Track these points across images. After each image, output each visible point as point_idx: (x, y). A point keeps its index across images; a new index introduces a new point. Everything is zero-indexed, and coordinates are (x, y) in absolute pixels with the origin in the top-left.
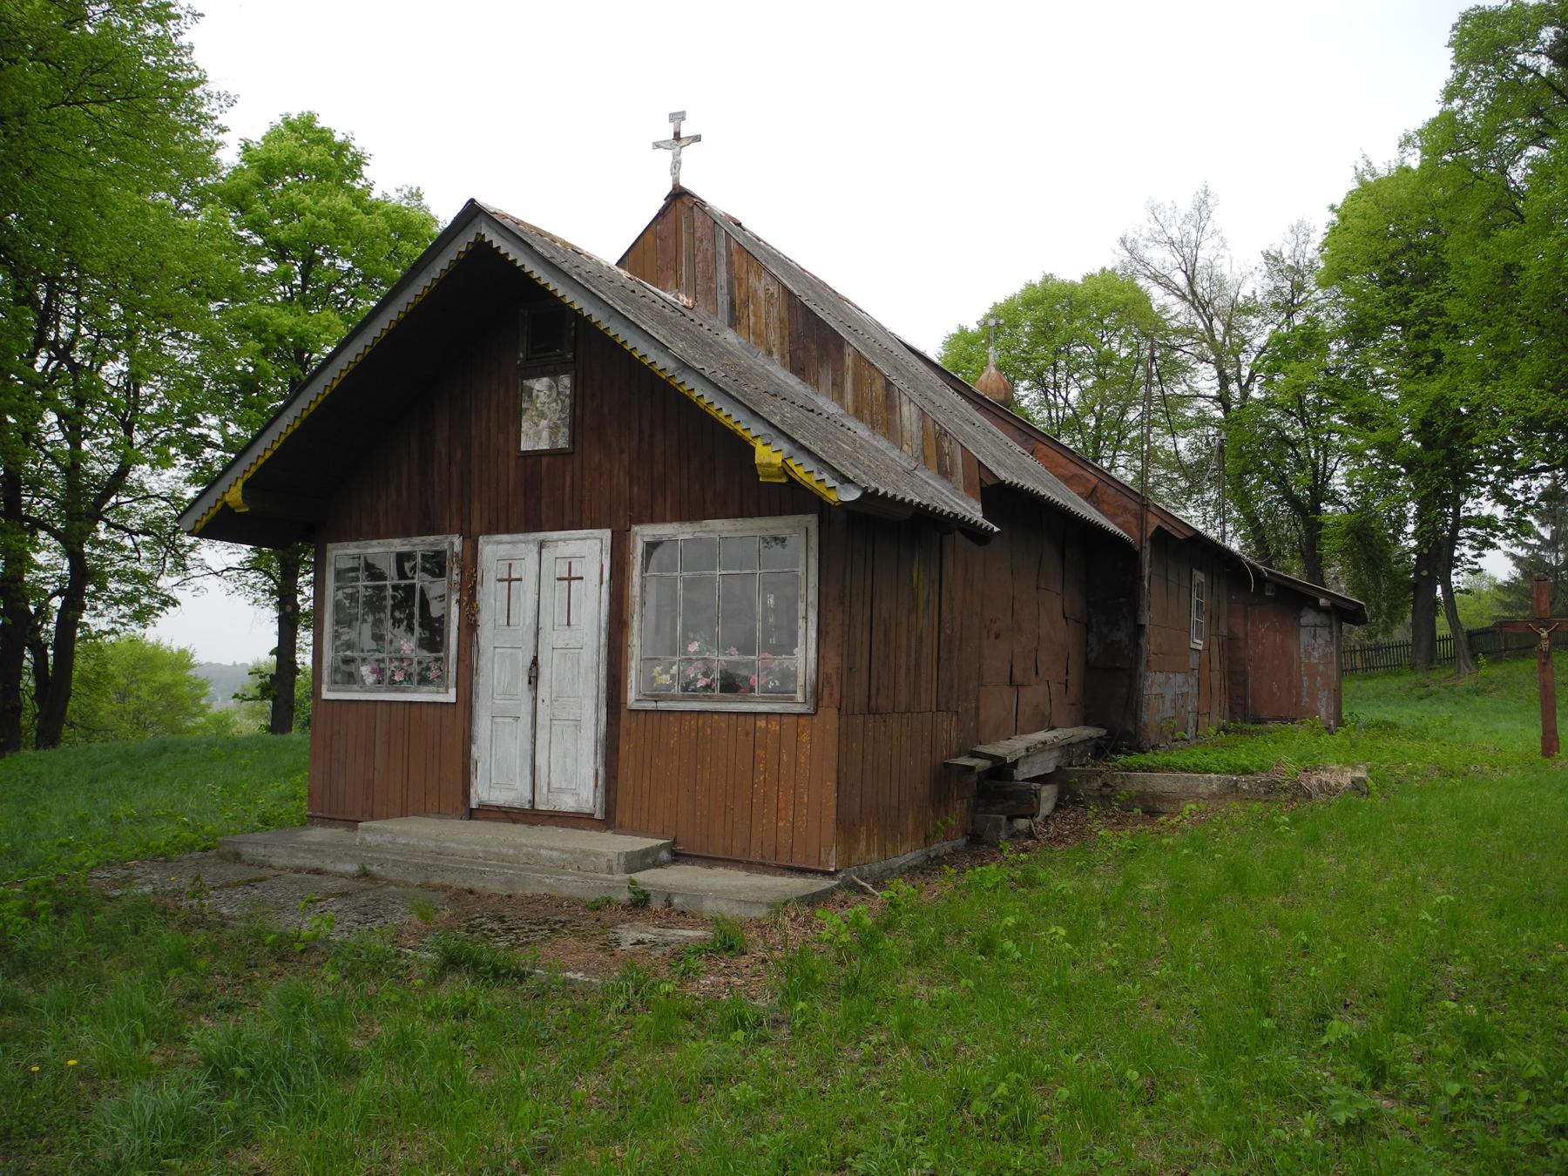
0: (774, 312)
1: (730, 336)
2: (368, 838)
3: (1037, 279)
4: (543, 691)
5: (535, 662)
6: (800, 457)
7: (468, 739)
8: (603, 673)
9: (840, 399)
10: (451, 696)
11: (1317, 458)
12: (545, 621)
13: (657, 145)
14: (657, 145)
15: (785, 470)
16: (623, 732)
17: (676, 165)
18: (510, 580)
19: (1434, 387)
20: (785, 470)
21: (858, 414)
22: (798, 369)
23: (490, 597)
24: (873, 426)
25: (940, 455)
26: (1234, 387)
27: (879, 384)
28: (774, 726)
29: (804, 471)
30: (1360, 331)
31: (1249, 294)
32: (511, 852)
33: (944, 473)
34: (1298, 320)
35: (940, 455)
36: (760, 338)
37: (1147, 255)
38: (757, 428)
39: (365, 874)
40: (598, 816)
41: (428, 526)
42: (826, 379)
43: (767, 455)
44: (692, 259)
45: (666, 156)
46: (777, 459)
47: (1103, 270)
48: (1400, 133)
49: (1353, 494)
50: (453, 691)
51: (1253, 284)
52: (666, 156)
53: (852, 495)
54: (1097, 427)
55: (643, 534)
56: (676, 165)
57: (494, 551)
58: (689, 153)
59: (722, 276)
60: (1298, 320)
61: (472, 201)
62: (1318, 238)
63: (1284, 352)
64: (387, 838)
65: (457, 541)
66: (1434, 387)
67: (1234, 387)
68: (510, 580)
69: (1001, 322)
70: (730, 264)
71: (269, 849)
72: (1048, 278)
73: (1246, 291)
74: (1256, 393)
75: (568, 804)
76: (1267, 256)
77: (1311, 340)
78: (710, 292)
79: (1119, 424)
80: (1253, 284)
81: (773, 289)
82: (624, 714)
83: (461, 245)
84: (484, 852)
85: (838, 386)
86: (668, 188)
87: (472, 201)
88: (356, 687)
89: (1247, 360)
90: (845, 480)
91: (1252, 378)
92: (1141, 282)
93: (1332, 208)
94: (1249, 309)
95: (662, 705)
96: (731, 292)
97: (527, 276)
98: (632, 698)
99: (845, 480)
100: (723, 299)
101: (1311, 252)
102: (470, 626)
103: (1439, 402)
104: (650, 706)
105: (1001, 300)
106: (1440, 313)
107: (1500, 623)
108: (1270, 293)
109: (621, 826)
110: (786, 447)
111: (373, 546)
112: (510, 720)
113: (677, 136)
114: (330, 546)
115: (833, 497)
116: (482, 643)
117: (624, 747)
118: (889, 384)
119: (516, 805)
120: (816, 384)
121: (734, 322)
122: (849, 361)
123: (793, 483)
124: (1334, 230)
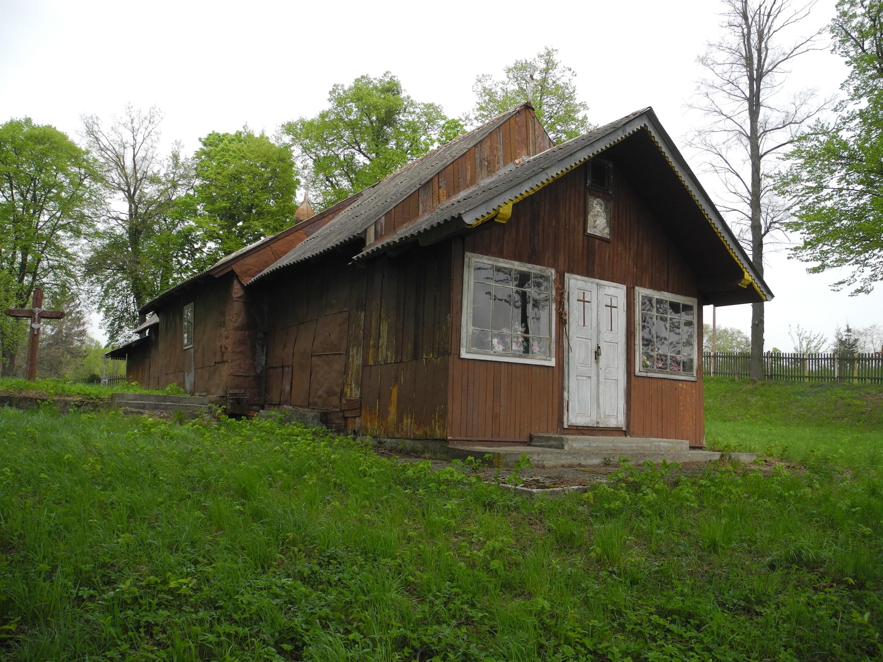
2: (575, 445)
6: (757, 281)
10: (552, 363)
16: (632, 386)
23: (574, 310)
31: (156, 171)
32: (648, 445)
39: (607, 464)
40: (624, 429)
41: (533, 259)
50: (554, 360)
51: (160, 166)
55: (641, 292)
61: (649, 114)
64: (586, 444)
65: (553, 271)
68: (611, 307)
71: (541, 455)
75: (613, 423)
80: (160, 166)
82: (633, 377)
84: (636, 446)
87: (649, 114)
93: (200, 139)
109: (633, 433)
111: (501, 262)
112: (585, 378)
114: (468, 254)
117: (633, 394)
119: (590, 425)
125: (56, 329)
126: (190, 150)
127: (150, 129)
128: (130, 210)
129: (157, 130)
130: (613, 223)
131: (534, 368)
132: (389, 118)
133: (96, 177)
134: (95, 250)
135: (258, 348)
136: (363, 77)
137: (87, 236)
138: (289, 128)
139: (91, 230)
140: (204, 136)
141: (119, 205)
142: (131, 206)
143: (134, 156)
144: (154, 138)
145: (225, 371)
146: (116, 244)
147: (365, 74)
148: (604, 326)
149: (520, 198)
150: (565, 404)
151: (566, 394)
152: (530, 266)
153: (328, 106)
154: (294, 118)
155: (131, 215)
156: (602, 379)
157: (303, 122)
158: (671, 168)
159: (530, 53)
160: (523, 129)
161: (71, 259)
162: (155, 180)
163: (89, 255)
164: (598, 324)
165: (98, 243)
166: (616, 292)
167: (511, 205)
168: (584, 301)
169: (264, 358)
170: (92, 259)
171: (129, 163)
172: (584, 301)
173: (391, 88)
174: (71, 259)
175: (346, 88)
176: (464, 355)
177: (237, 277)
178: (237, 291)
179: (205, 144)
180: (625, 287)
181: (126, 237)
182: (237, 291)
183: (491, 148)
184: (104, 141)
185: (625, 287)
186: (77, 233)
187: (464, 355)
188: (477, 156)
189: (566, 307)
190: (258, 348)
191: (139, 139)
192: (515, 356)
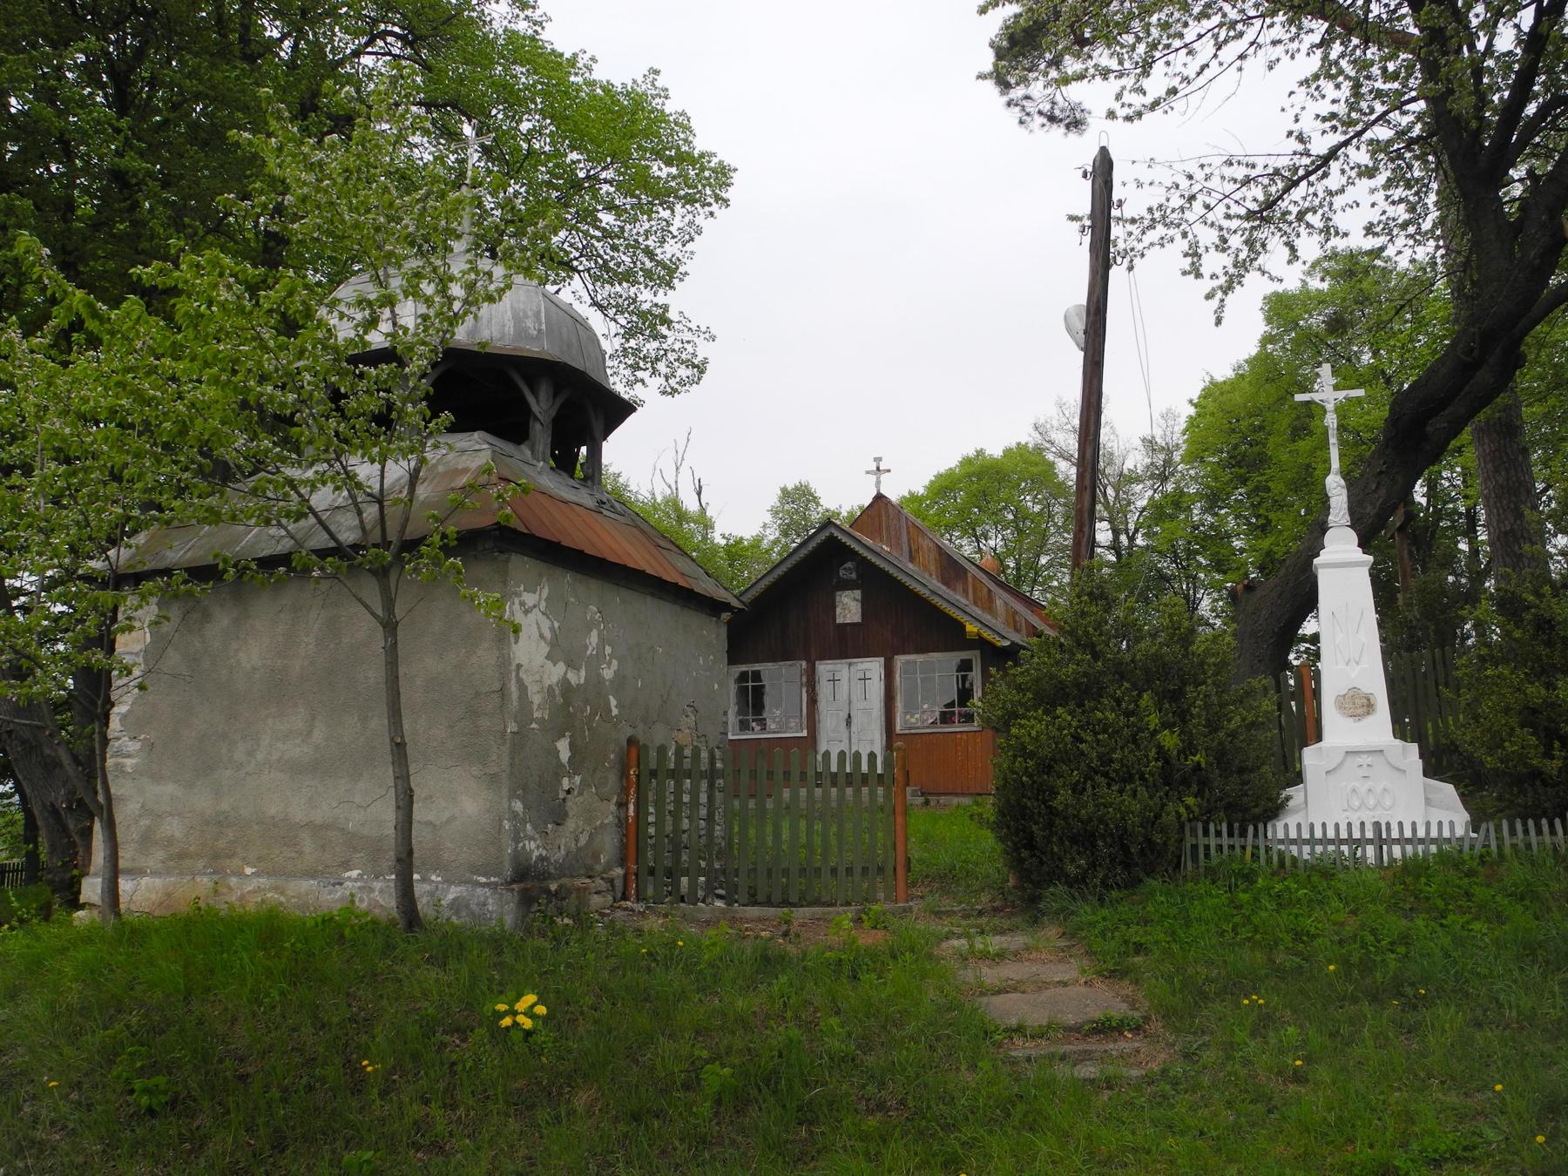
0: (932, 556)
1: (910, 566)
3: (971, 453)
4: (854, 728)
5: (849, 716)
6: (985, 629)
8: (883, 719)
9: (967, 597)
10: (805, 734)
11: (1188, 589)
12: (854, 698)
13: (868, 472)
14: (868, 472)
15: (978, 634)
17: (878, 483)
18: (834, 681)
19: (1265, 544)
20: (978, 634)
21: (975, 603)
22: (946, 582)
23: (824, 689)
24: (983, 609)
25: (1015, 622)
26: (1123, 538)
27: (985, 590)
28: (965, 737)
29: (987, 634)
30: (1213, 500)
33: (1017, 630)
34: (1170, 487)
35: (1015, 622)
36: (926, 568)
37: (1054, 436)
42: (960, 587)
43: (971, 628)
44: (888, 528)
45: (874, 478)
46: (975, 630)
47: (1019, 444)
48: (1234, 362)
49: (1217, 616)
52: (874, 478)
53: (1007, 643)
54: (1018, 568)
55: (900, 660)
56: (878, 483)
58: (884, 477)
59: (905, 538)
60: (1170, 487)
62: (1182, 424)
63: (1159, 512)
66: (1265, 544)
67: (1123, 538)
69: (944, 487)
70: (908, 532)
72: (980, 453)
73: (1129, 465)
74: (1140, 541)
77: (1178, 502)
78: (899, 545)
79: (1034, 566)
81: (931, 545)
83: (822, 537)
85: (965, 591)
86: (874, 493)
89: (1133, 519)
90: (1004, 637)
91: (1136, 531)
92: (1050, 457)
93: (1191, 401)
94: (1133, 478)
96: (910, 546)
98: (898, 728)
99: (1004, 637)
100: (905, 547)
101: (1178, 438)
103: (1269, 553)
105: (942, 470)
106: (1268, 490)
107: (1541, 773)
108: (1148, 467)
113: (878, 469)
115: (999, 644)
116: (821, 708)
118: (990, 590)
120: (955, 590)
121: (912, 559)
122: (970, 580)
123: (981, 638)
124: (1192, 421)
168: (834, 681)
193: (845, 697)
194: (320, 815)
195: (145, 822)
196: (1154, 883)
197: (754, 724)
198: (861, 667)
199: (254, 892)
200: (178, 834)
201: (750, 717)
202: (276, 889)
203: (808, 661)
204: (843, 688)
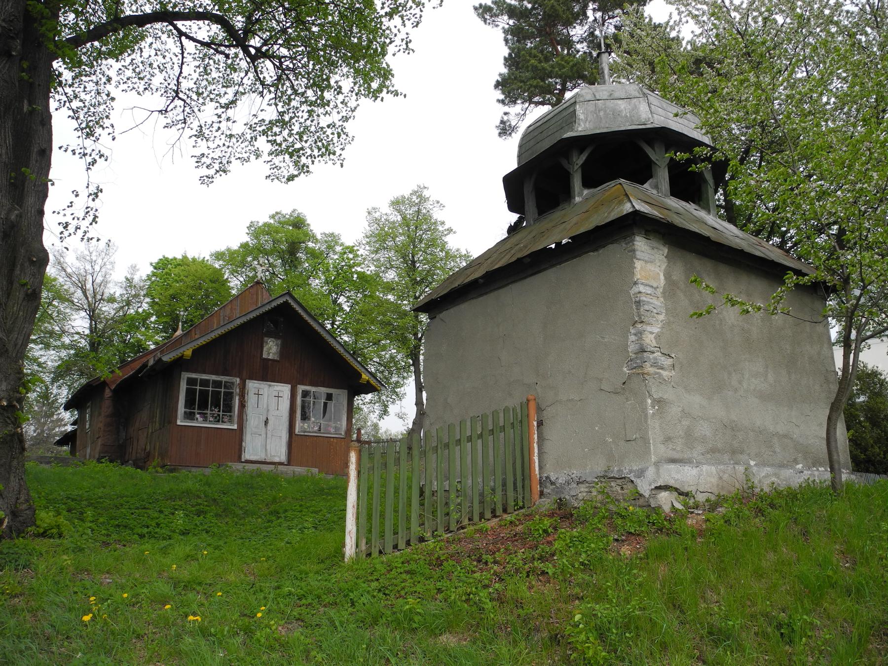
6: (372, 379)
7: (241, 440)
10: (235, 427)
15: (368, 382)
20: (368, 382)
23: (251, 399)
28: (335, 441)
38: (363, 370)
41: (225, 373)
46: (367, 378)
51: (115, 290)
55: (301, 388)
57: (252, 385)
65: (238, 380)
68: (278, 397)
75: (277, 460)
76: (127, 279)
80: (115, 290)
82: (294, 435)
83: (281, 301)
88: (195, 421)
93: (151, 264)
95: (306, 434)
97: (301, 316)
98: (297, 430)
102: (243, 406)
104: (302, 434)
110: (370, 376)
125: (39, 431)
126: (145, 271)
127: (105, 260)
128: (91, 325)
129: (112, 259)
130: (283, 352)
131: (203, 429)
132: (293, 248)
133: (63, 299)
134: (61, 358)
135: (121, 427)
136: (277, 213)
137: (56, 348)
138: (218, 256)
139: (59, 343)
140: (155, 260)
141: (80, 323)
142: (91, 322)
143: (93, 282)
144: (109, 267)
145: (100, 442)
146: (80, 353)
147: (278, 211)
148: (273, 406)
149: (197, 346)
150: (243, 449)
151: (244, 444)
152: (223, 377)
153: (246, 239)
154: (222, 248)
155: (91, 331)
156: (269, 435)
157: (228, 250)
158: (306, 321)
159: (405, 190)
160: (255, 296)
161: (43, 368)
162: (111, 300)
163: (56, 364)
164: (268, 406)
165: (64, 353)
166: (285, 389)
167: (191, 350)
168: (258, 394)
169: (124, 434)
170: (59, 366)
171: (89, 286)
172: (258, 394)
173: (298, 223)
174: (43, 368)
175: (260, 224)
176: (179, 423)
177: (108, 385)
178: (108, 393)
179: (155, 268)
180: (290, 386)
181: (88, 347)
182: (108, 393)
183: (231, 309)
184: (69, 270)
185: (290, 386)
186: (47, 346)
187: (179, 423)
188: (221, 314)
189: (246, 398)
190: (121, 427)
191: (97, 268)
192: (315, 432)
193: (265, 406)
194: (781, 429)
195: (686, 423)
196: (767, 489)
197: (198, 416)
198: (276, 388)
199: (765, 477)
200: (708, 434)
201: (196, 411)
202: (775, 475)
203: (241, 379)
204: (264, 400)
